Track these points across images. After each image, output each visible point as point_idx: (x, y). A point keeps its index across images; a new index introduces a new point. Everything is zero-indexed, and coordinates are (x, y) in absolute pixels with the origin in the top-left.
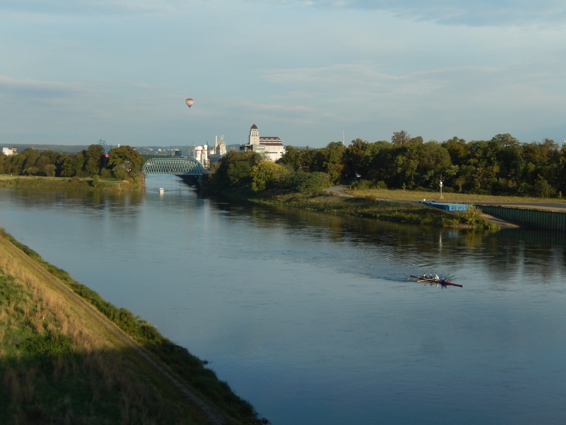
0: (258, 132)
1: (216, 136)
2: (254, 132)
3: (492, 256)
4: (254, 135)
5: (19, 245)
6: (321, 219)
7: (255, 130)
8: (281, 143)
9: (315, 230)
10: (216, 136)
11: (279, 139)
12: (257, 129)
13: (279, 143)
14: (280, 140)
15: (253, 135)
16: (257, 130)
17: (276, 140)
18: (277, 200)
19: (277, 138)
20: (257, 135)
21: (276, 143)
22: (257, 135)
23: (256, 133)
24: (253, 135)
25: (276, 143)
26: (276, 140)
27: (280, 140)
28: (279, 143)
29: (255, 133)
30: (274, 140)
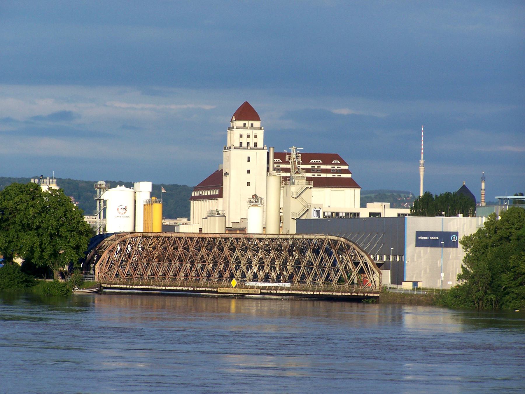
0: (261, 134)
1: (303, 148)
2: (245, 132)
3: (108, 292)
4: (245, 145)
5: (135, 197)
6: (463, 318)
7: (248, 123)
8: (349, 176)
9: (484, 325)
10: (303, 148)
11: (343, 163)
12: (257, 119)
13: (344, 176)
14: (346, 167)
15: (241, 144)
16: (257, 124)
17: (329, 167)
18: (516, 294)
19: (336, 157)
20: (256, 144)
21: (330, 175)
22: (256, 144)
23: (245, 136)
24: (241, 144)
25: (330, 175)
26: (329, 167)
27: (346, 167)
28: (344, 176)
29: (248, 136)
30: (323, 167)
